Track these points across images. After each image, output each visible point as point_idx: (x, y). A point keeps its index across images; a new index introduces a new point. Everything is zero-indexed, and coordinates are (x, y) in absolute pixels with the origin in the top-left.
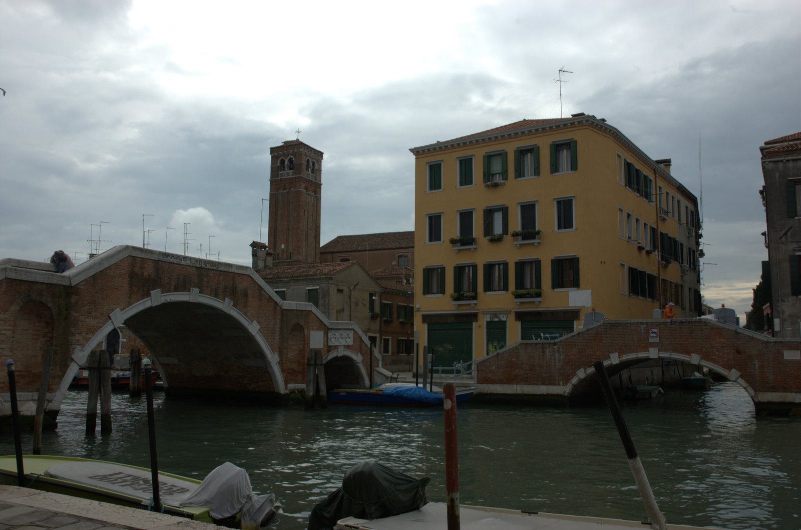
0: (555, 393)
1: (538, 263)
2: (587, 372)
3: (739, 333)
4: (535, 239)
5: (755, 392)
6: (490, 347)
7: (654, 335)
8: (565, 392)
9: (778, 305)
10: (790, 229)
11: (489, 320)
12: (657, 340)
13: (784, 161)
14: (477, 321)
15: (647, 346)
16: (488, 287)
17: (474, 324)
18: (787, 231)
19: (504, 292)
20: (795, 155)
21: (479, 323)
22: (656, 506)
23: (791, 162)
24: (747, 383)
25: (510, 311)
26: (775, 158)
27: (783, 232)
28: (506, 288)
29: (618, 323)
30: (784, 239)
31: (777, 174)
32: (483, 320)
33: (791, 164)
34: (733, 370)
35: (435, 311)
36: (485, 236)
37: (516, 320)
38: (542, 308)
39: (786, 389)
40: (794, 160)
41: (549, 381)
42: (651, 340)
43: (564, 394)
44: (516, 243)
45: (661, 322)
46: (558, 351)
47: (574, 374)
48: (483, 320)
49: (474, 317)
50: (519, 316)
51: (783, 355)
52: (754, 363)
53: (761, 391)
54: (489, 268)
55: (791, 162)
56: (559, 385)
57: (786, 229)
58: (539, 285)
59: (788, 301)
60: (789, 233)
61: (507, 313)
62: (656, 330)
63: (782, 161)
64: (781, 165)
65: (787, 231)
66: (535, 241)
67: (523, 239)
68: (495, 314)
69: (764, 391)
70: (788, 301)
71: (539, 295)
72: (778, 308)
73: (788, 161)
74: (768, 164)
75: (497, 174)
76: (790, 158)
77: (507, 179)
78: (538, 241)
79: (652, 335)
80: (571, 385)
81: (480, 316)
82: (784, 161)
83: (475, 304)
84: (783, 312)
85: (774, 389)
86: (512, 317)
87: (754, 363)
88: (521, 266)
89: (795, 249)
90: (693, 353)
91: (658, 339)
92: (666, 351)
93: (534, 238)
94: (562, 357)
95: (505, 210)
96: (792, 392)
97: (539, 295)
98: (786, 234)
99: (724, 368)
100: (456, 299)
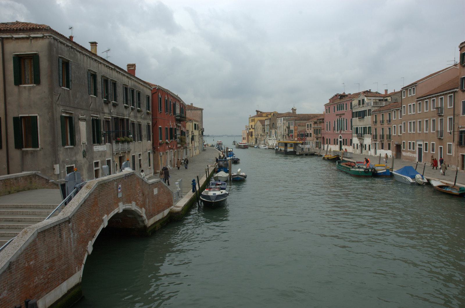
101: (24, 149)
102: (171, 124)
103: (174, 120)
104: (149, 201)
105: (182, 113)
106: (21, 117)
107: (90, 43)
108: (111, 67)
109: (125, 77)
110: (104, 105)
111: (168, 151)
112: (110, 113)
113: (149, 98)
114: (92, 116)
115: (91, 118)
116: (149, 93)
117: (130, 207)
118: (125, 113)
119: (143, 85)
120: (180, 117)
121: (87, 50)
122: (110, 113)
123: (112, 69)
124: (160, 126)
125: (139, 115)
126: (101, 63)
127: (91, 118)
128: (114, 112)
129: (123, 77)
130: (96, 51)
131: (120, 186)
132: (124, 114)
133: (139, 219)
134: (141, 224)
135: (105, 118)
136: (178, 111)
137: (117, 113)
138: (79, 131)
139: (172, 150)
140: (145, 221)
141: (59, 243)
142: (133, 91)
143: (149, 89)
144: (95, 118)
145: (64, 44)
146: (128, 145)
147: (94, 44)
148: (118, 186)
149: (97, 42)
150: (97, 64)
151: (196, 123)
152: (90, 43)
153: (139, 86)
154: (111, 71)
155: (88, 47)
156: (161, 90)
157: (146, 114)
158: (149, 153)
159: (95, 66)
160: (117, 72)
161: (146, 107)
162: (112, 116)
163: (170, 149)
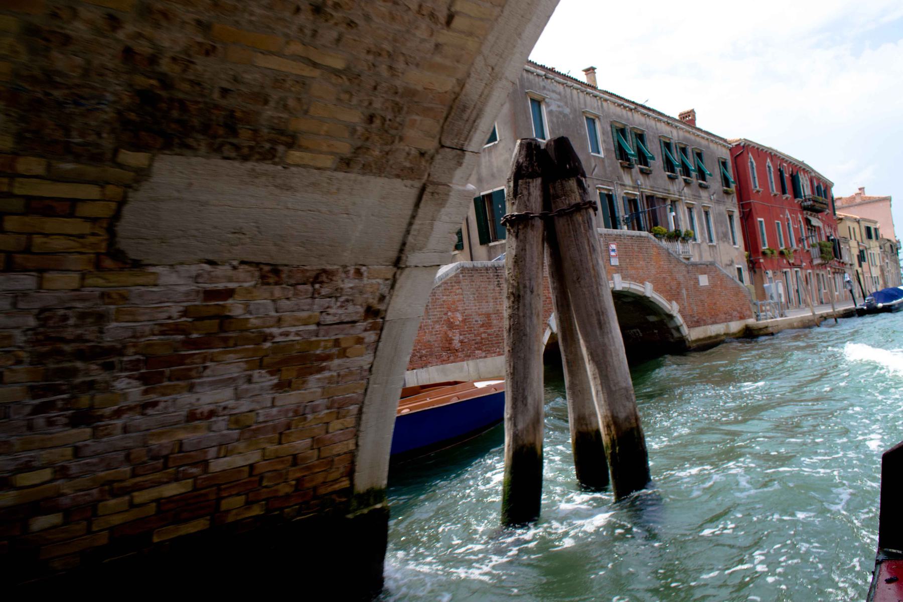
101: (492, 244)
102: (789, 217)
103: (797, 209)
104: (688, 295)
105: (818, 195)
106: (483, 196)
107: (584, 71)
108: (628, 107)
109: (663, 124)
110: (621, 171)
111: (788, 270)
112: (636, 187)
113: (724, 164)
114: (599, 188)
115: (598, 191)
116: (726, 155)
117: (642, 290)
118: (671, 188)
119: (707, 139)
120: (814, 201)
121: (582, 83)
122: (636, 187)
123: (631, 110)
124: (759, 219)
125: (704, 194)
126: (606, 100)
127: (598, 191)
128: (647, 186)
129: (658, 124)
130: (595, 81)
131: (613, 246)
132: (669, 190)
133: (671, 325)
134: (676, 335)
135: (626, 193)
136: (806, 191)
137: (651, 187)
138: (635, 290)
139: (798, 269)
140: (681, 328)
141: (498, 294)
142: (684, 150)
143: (724, 146)
144: (606, 192)
145: (532, 73)
146: (684, 246)
147: (590, 71)
148: (608, 246)
149: (594, 66)
150: (599, 102)
151: (868, 224)
152: (584, 71)
153: (698, 139)
154: (629, 114)
155: (583, 78)
156: (754, 147)
157: (722, 193)
158: (739, 270)
159: (596, 105)
160: (644, 114)
161: (720, 180)
162: (642, 192)
163: (792, 265)
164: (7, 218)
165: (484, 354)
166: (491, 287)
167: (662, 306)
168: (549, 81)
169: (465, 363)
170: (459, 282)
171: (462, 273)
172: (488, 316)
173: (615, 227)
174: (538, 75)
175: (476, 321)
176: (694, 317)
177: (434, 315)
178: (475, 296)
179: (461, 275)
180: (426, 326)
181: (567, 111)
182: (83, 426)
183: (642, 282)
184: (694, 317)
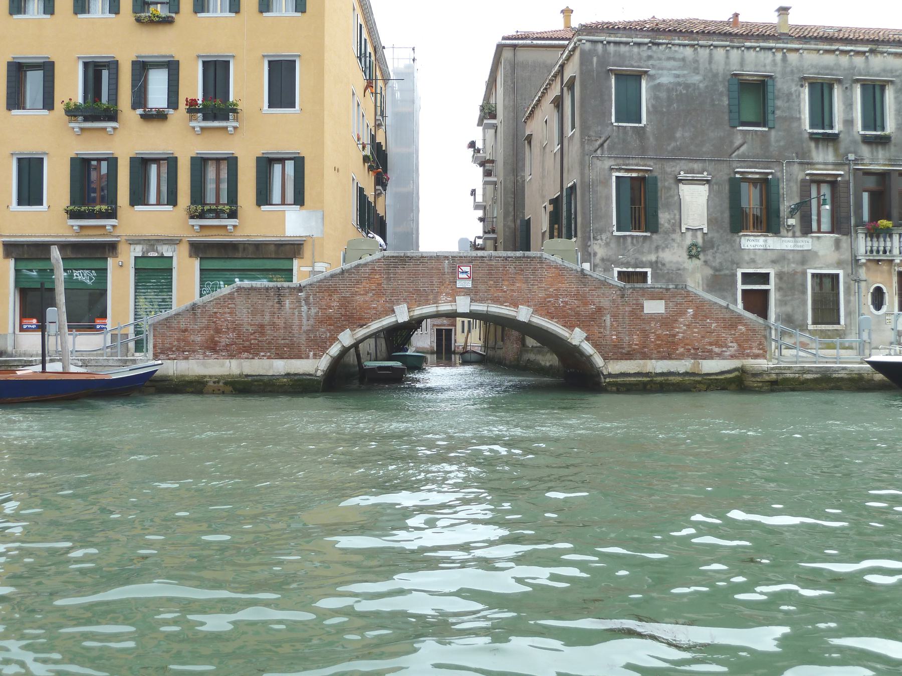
0: (301, 371)
1: (232, 162)
2: (356, 337)
3: (587, 275)
4: (228, 119)
5: (604, 360)
6: (142, 300)
7: (465, 276)
8: (317, 370)
9: (589, 244)
10: (607, 140)
11: (140, 255)
12: (469, 284)
13: (605, 42)
14: (115, 256)
15: (455, 292)
16: (139, 197)
17: (110, 260)
18: (605, 141)
19: (170, 208)
20: (619, 35)
21: (121, 258)
22: (804, 551)
23: (612, 44)
24: (595, 348)
25: (180, 241)
26: (594, 36)
27: (599, 142)
28: (172, 200)
29: (408, 257)
30: (599, 152)
31: (595, 59)
32: (129, 255)
33: (612, 48)
34: (577, 330)
35: (31, 236)
36: (134, 107)
37: (191, 256)
38: (239, 237)
39: (645, 356)
40: (616, 43)
41: (293, 352)
42: (460, 284)
43: (316, 371)
44: (193, 124)
45: (475, 257)
46: (307, 300)
47: (334, 339)
48: (129, 255)
49: (111, 248)
50: (198, 249)
51: (643, 307)
52: (605, 318)
53: (612, 359)
54: (141, 165)
55: (612, 44)
56: (308, 357)
57: (603, 139)
58: (233, 197)
59: (602, 239)
60: (606, 145)
61: (173, 242)
62: (467, 269)
63: (602, 42)
64: (600, 47)
65: (605, 141)
66: (230, 124)
67: (205, 119)
68: (152, 243)
69: (617, 359)
70: (602, 239)
71: (233, 215)
72: (589, 249)
73: (609, 43)
74: (584, 43)
75: (157, 3)
76: (612, 39)
77: (177, 12)
78: (236, 124)
79: (461, 276)
80: (328, 357)
81: (122, 248)
82: (605, 42)
83: (114, 226)
84: (595, 254)
85: (629, 356)
86: (184, 249)
87: (605, 318)
88: (200, 164)
89: (612, 167)
90: (522, 304)
91: (471, 282)
92: (481, 300)
93: (227, 119)
94: (313, 311)
95: (172, 67)
96: (651, 359)
97: (233, 215)
98: (602, 145)
99: (564, 326)
100: (73, 215)
164: (281, 165)
165: (251, 356)
166: (270, 303)
167: (554, 333)
168: (662, 48)
169: (228, 361)
170: (234, 299)
171: (237, 292)
172: (262, 326)
173: (496, 250)
174: (639, 44)
175: (247, 330)
176: (623, 348)
177: (201, 322)
178: (249, 310)
179: (236, 294)
180: (192, 330)
181: (696, 79)
182: (843, 374)
183: (516, 306)
184: (623, 348)
